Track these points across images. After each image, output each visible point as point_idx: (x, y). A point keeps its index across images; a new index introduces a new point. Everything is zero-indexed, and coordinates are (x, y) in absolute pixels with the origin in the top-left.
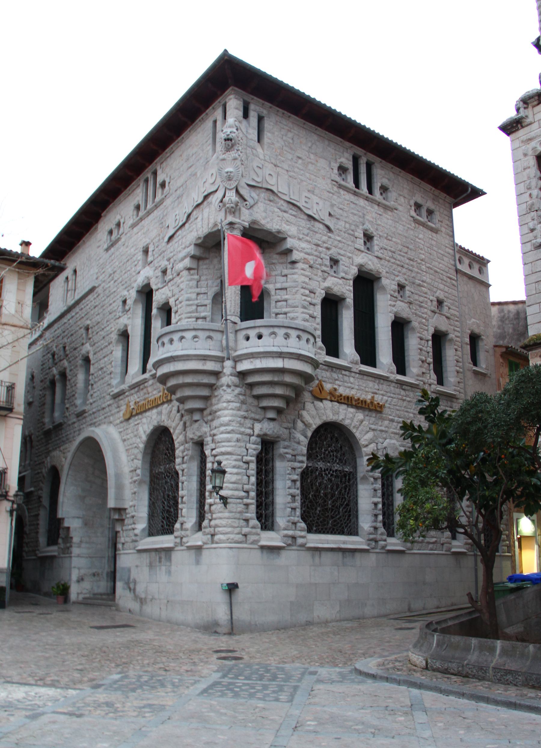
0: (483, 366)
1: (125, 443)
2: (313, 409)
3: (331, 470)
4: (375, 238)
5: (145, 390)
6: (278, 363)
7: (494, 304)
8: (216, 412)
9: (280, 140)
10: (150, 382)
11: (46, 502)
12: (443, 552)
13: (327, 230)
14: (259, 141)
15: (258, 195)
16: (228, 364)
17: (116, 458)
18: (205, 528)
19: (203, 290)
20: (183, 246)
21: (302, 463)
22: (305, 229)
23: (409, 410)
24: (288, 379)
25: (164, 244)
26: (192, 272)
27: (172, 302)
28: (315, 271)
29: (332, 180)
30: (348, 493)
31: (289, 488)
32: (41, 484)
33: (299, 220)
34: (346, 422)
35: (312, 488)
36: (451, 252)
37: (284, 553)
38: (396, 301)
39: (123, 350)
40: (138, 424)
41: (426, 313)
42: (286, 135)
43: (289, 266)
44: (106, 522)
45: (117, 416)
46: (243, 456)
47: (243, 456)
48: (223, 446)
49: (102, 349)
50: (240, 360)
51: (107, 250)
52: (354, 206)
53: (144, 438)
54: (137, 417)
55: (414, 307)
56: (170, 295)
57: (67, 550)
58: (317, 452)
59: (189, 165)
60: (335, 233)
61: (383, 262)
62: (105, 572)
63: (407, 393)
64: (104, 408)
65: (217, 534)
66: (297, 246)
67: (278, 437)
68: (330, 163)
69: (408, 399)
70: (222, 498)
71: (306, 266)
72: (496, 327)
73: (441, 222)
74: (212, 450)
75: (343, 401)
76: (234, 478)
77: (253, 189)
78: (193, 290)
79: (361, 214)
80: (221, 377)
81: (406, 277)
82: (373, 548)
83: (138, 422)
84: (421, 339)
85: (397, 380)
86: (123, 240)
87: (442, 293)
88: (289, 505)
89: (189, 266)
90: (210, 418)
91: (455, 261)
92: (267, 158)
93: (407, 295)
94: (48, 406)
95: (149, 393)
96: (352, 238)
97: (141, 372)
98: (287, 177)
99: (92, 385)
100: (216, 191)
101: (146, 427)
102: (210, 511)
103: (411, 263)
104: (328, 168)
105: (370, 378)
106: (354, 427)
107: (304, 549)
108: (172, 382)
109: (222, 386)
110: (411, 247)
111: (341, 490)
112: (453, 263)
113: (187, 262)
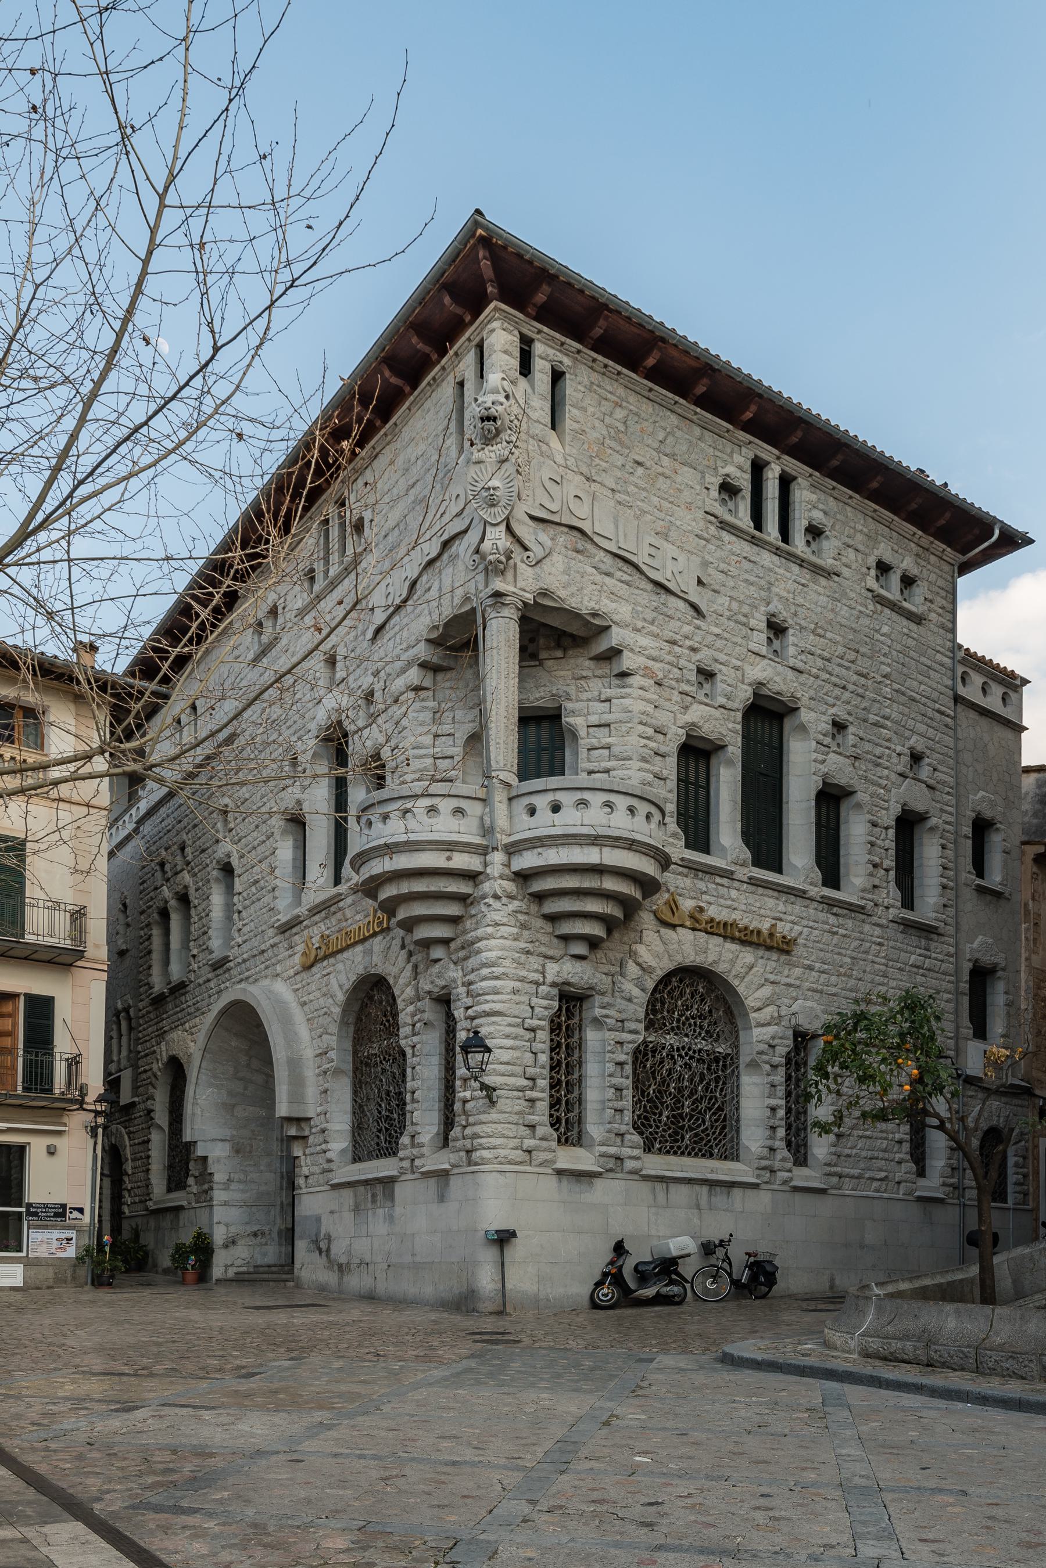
0: (995, 878)
1: (306, 1008)
2: (658, 942)
3: (689, 1049)
4: (791, 631)
5: (339, 915)
6: (591, 856)
7: (1028, 770)
8: (473, 943)
9: (597, 423)
10: (349, 900)
11: (161, 1117)
12: (900, 1196)
13: (692, 612)
14: (553, 428)
15: (552, 539)
16: (498, 858)
17: (291, 1037)
18: (456, 1140)
19: (446, 728)
20: (404, 646)
21: (636, 1035)
22: (647, 610)
23: (843, 951)
24: (610, 884)
25: (365, 644)
26: (423, 694)
27: (386, 753)
28: (666, 693)
29: (706, 512)
30: (722, 1090)
31: (611, 1075)
32: (151, 1090)
33: (637, 591)
34: (721, 968)
35: (655, 1078)
36: (947, 661)
37: (598, 1182)
38: (827, 754)
39: (295, 847)
40: (328, 974)
41: (887, 778)
42: (611, 415)
43: (615, 681)
44: (275, 1147)
45: (289, 963)
46: (524, 1019)
47: (524, 1019)
48: (487, 1002)
49: (255, 848)
50: (519, 852)
51: (256, 660)
52: (750, 566)
53: (341, 997)
54: (325, 963)
55: (862, 765)
56: (382, 740)
57: (205, 1196)
58: (664, 1018)
59: (411, 482)
60: (709, 619)
61: (803, 678)
62: (276, 1230)
63: (841, 920)
64: (263, 952)
65: (477, 1150)
66: (631, 642)
67: (591, 988)
68: (703, 477)
69: (842, 931)
70: (484, 1087)
71: (649, 682)
72: (1030, 814)
73: (931, 601)
74: (467, 1008)
75: (714, 930)
76: (506, 1056)
77: (541, 526)
78: (426, 729)
79: (763, 582)
80: (482, 882)
81: (849, 707)
82: (767, 1183)
83: (328, 971)
84: (875, 825)
85: (822, 897)
86: (284, 642)
87: (922, 740)
88: (610, 1104)
89: (416, 682)
90: (461, 954)
91: (953, 679)
92: (571, 462)
93: (851, 743)
94: (156, 957)
95: (346, 920)
96: (745, 630)
97: (332, 885)
98: (612, 503)
99: (240, 912)
100: (465, 531)
101: (343, 978)
102: (465, 1112)
103: (863, 681)
104: (698, 487)
105: (770, 892)
106: (736, 976)
107: (637, 1177)
108: (388, 892)
109: (483, 897)
110: (862, 650)
111: (708, 1084)
112: (950, 683)
113: (414, 675)
